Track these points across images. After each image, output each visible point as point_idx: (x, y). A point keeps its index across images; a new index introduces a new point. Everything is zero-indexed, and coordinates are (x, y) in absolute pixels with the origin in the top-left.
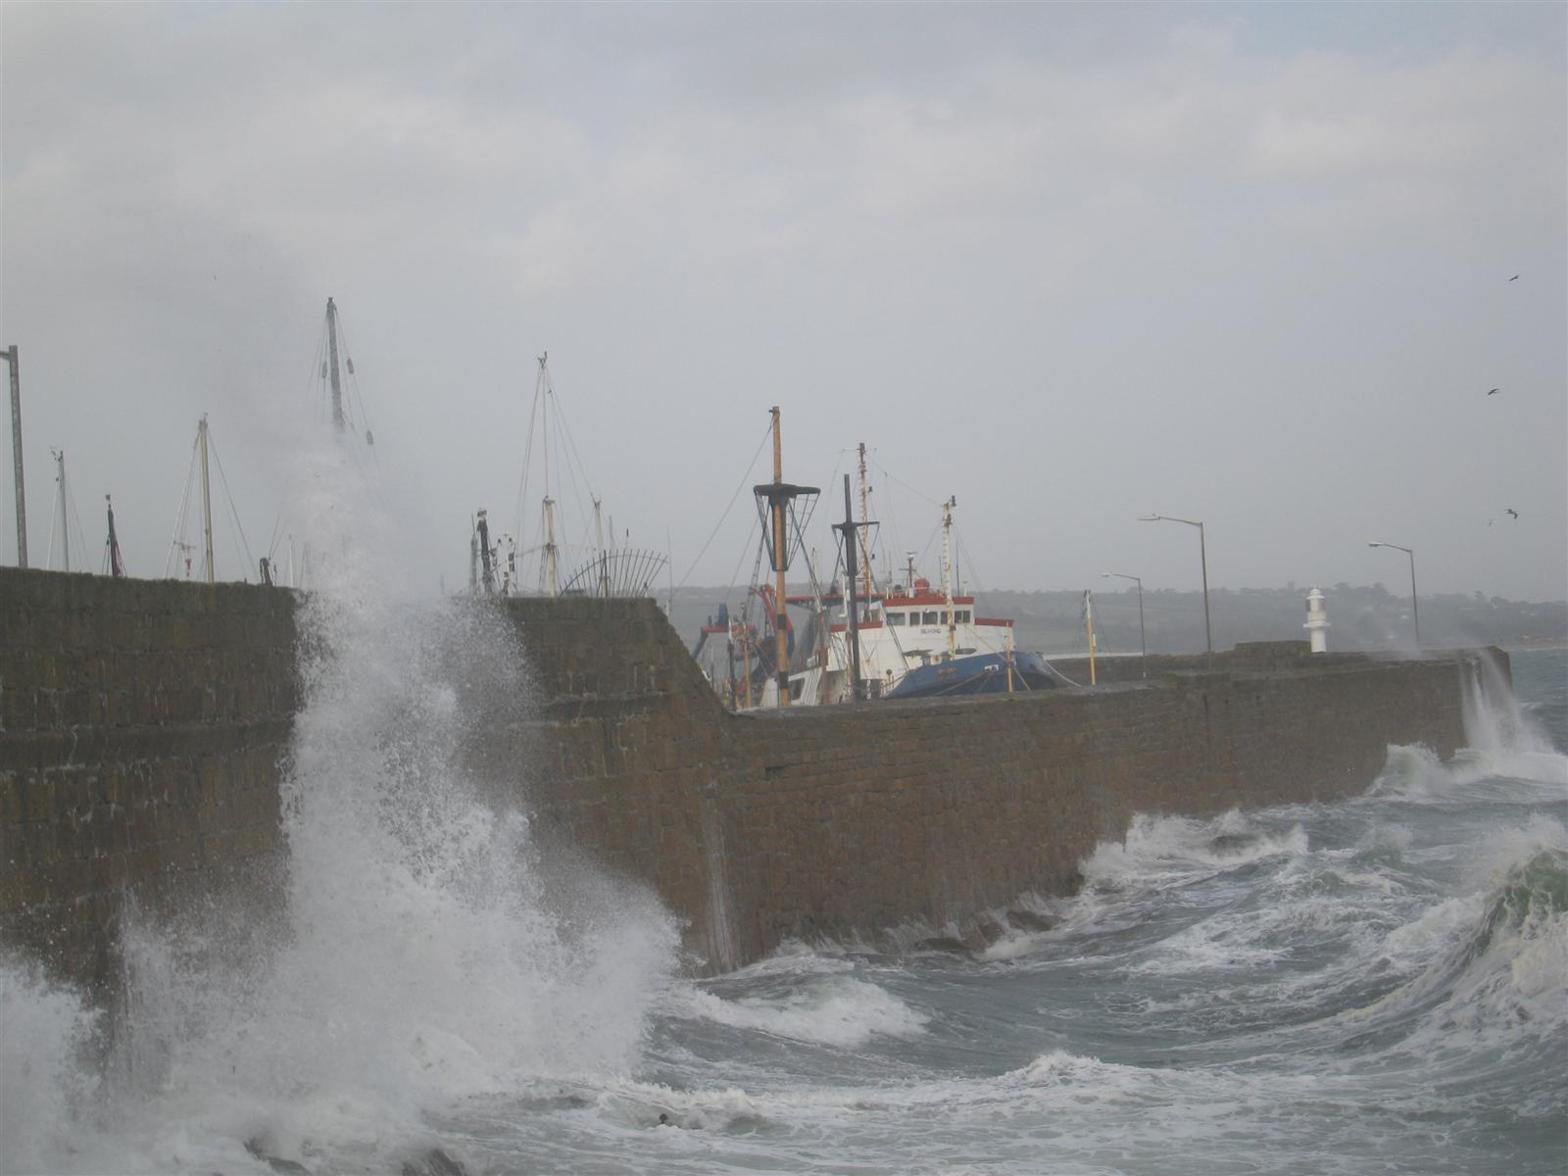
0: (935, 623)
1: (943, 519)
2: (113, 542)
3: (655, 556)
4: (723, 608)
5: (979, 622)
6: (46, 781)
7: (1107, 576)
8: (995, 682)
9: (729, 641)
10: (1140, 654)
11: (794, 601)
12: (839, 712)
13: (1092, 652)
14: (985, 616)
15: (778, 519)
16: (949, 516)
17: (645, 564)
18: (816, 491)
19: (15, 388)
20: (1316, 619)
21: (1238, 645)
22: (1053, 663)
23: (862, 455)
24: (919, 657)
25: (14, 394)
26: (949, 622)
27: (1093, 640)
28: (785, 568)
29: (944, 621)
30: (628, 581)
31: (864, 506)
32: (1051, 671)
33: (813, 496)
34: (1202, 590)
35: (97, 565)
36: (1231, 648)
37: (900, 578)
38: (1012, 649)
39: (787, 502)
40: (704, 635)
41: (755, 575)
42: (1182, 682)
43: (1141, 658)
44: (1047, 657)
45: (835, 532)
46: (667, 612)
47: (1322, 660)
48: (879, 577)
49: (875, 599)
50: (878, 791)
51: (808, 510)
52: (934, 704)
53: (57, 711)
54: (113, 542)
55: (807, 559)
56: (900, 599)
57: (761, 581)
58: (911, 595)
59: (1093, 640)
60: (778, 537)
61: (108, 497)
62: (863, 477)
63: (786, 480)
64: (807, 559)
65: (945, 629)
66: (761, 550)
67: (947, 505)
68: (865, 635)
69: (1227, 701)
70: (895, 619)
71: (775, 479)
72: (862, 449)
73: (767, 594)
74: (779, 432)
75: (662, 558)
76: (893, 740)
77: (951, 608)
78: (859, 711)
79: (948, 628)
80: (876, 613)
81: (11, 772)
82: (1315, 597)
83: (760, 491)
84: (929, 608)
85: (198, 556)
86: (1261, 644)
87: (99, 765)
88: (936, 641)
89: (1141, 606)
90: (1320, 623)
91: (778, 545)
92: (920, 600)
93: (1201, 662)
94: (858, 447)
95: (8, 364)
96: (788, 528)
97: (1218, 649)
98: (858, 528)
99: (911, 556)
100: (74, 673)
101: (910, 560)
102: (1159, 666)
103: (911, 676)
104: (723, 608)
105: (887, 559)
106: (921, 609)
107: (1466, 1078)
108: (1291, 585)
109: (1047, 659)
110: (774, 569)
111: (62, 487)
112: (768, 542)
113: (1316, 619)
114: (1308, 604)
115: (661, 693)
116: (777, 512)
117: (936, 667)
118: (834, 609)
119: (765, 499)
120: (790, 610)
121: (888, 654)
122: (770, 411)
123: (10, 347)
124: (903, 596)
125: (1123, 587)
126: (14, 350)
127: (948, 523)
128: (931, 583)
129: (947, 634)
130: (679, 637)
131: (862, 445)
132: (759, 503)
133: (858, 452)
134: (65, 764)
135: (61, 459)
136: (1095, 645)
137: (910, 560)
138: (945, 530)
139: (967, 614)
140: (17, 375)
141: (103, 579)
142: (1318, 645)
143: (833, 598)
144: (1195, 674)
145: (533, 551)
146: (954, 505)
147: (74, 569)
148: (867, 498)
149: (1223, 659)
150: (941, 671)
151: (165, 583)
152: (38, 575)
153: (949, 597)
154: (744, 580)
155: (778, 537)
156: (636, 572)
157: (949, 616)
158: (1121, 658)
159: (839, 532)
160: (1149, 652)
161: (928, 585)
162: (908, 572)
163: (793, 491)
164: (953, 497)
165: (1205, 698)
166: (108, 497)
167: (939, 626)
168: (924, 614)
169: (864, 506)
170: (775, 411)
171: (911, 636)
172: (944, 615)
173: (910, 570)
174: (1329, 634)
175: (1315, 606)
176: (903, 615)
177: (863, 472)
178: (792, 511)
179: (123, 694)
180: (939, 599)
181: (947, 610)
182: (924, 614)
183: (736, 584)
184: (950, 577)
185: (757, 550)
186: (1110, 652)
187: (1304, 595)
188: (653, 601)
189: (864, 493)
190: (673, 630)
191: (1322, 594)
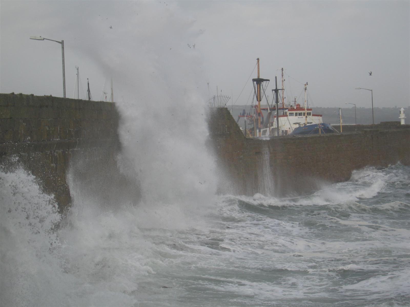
0: (302, 115)
1: (304, 88)
2: (89, 91)
3: (227, 97)
4: (244, 111)
5: (313, 115)
6: (70, 153)
7: (347, 104)
8: (316, 131)
9: (245, 120)
10: (355, 124)
11: (264, 109)
12: (275, 138)
13: (341, 124)
14: (314, 114)
15: (258, 87)
16: (306, 87)
17: (226, 99)
18: (269, 80)
19: (63, 51)
20: (402, 116)
21: (381, 122)
22: (334, 126)
23: (282, 71)
24: (298, 125)
25: (63, 53)
26: (306, 115)
27: (341, 121)
28: (260, 100)
29: (304, 115)
30: (219, 103)
31: (283, 85)
32: (333, 128)
33: (268, 82)
34: (372, 108)
35: (84, 97)
36: (379, 123)
37: (292, 104)
38: (322, 123)
39: (261, 83)
40: (239, 117)
41: (253, 102)
42: (366, 131)
43: (355, 125)
44: (332, 125)
45: (273, 91)
46: (231, 112)
47: (404, 126)
48: (286, 102)
49: (286, 109)
50: (285, 159)
51: (266, 85)
52: (300, 137)
53: (73, 135)
54: (89, 91)
55: (266, 98)
56: (292, 109)
57: (254, 104)
58: (295, 108)
59: (341, 121)
60: (258, 92)
61: (88, 79)
62: (282, 77)
63: (261, 77)
64: (266, 98)
65: (304, 117)
66: (254, 96)
67: (305, 85)
68: (281, 119)
69: (378, 137)
70: (291, 114)
71: (258, 77)
72: (282, 69)
73: (257, 107)
74: (259, 65)
75: (229, 97)
76: (289, 146)
77: (306, 112)
78: (280, 138)
79: (305, 117)
80: (286, 113)
81: (61, 150)
82: (402, 110)
83: (254, 80)
84: (300, 112)
85: (109, 96)
86: (387, 122)
87: (84, 149)
88: (302, 120)
89: (355, 112)
90: (403, 117)
91: (259, 94)
92: (298, 109)
93: (371, 127)
94: (281, 69)
95: (61, 45)
96: (261, 90)
97: (376, 123)
98: (279, 90)
99: (295, 98)
100: (77, 125)
101: (295, 99)
102: (359, 127)
103: (296, 129)
104: (244, 111)
105: (288, 98)
106: (298, 112)
107: (355, 292)
108: (396, 107)
109: (331, 126)
110: (257, 101)
111: (78, 76)
112: (256, 93)
113: (402, 116)
114: (400, 111)
115: (228, 133)
116: (258, 86)
117: (303, 127)
118: (273, 112)
119: (255, 83)
120: (263, 111)
121: (288, 124)
122: (257, 59)
123: (62, 41)
124: (293, 108)
125: (351, 106)
126: (63, 41)
127: (306, 89)
128: (301, 105)
129: (305, 118)
130: (233, 118)
131: (282, 68)
132: (254, 83)
133: (281, 70)
134: (75, 148)
135: (78, 69)
136: (342, 122)
137: (295, 99)
138: (305, 91)
139: (310, 113)
140: (64, 48)
141: (85, 101)
142: (403, 123)
143: (273, 109)
144: (369, 130)
145: (211, 99)
146: (307, 84)
147: (80, 98)
148: (283, 82)
149: (377, 126)
150: (303, 128)
151: (101, 102)
152: (68, 99)
153: (306, 109)
154: (250, 103)
155: (258, 92)
156: (224, 101)
157: (305, 114)
158: (350, 126)
159: (274, 92)
160: (357, 124)
161: (300, 106)
162: (294, 102)
163: (263, 80)
164: (307, 82)
165: (372, 136)
166: (88, 79)
167: (303, 116)
168: (299, 113)
169: (283, 85)
170: (258, 59)
171: (294, 119)
172: (304, 114)
173: (295, 101)
174: (406, 120)
175: (402, 112)
176: (293, 113)
177: (282, 76)
178: (262, 86)
179: (90, 131)
180: (304, 110)
181: (305, 112)
182: (299, 113)
183: (247, 105)
184: (306, 103)
185: (253, 96)
186: (346, 123)
187: (399, 109)
188: (226, 109)
189: (283, 81)
190: (232, 116)
191: (404, 109)
